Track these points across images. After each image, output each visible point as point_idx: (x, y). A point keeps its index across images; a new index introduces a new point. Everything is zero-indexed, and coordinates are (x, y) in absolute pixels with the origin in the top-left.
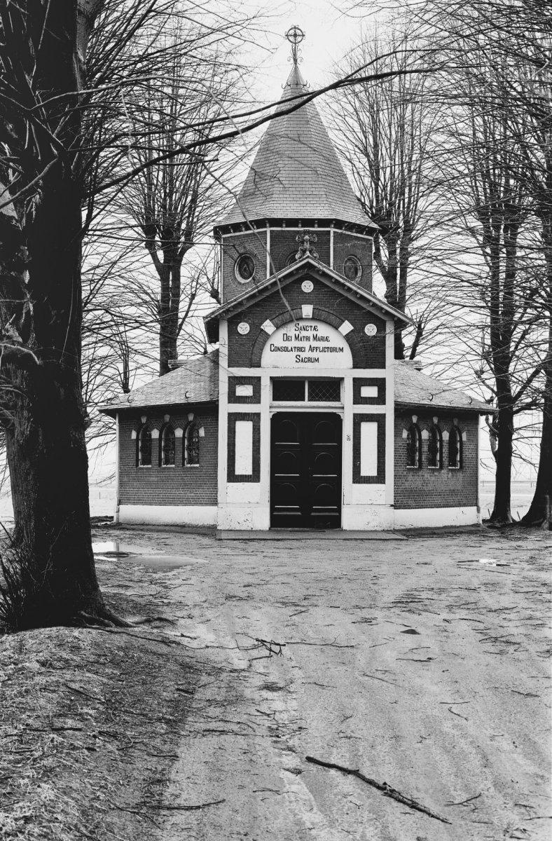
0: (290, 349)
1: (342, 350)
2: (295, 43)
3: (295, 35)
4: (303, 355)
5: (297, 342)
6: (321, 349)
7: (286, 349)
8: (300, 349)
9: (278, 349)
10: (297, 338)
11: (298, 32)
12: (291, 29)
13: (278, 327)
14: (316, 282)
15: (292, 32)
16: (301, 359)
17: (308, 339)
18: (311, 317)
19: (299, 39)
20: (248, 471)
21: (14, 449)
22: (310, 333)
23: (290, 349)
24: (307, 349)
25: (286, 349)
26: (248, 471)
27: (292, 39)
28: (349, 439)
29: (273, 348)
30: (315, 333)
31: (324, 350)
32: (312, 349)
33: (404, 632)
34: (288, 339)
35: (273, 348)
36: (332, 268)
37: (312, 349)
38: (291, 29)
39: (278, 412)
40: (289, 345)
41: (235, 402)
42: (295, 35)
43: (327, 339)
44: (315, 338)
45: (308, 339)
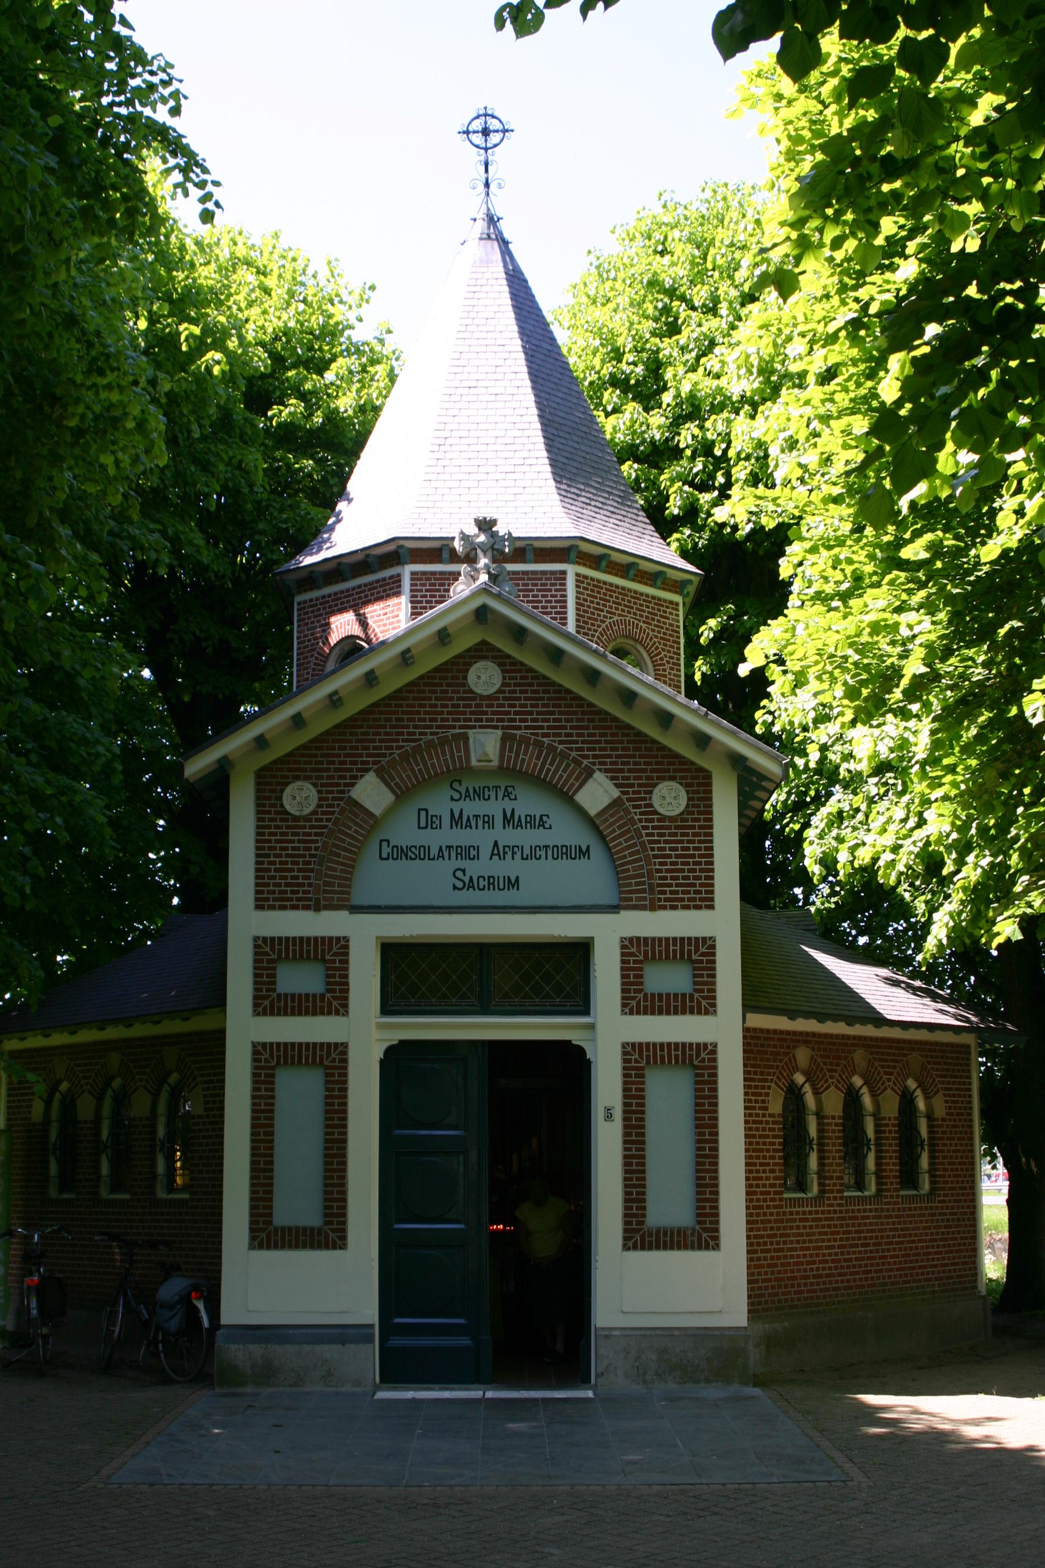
0: (434, 851)
1: (584, 853)
2: (486, 149)
3: (486, 132)
4: (475, 869)
5: (509, 830)
6: (527, 851)
7: (422, 853)
8: (467, 852)
9: (403, 853)
10: (456, 820)
11: (494, 124)
12: (477, 117)
13: (402, 794)
14: (502, 660)
15: (477, 125)
16: (467, 880)
17: (488, 821)
18: (495, 763)
19: (494, 138)
20: (310, 1215)
21: (744, 830)
22: (494, 807)
23: (434, 851)
24: (486, 850)
25: (422, 853)
26: (310, 1215)
27: (478, 139)
28: (609, 1116)
29: (386, 850)
30: (508, 805)
31: (533, 854)
32: (498, 851)
33: (886, 979)
34: (431, 822)
35: (386, 850)
36: (571, 627)
37: (498, 851)
38: (477, 117)
39: (402, 1043)
40: (434, 839)
41: (283, 1011)
42: (486, 132)
43: (541, 823)
44: (509, 820)
45: (488, 821)
